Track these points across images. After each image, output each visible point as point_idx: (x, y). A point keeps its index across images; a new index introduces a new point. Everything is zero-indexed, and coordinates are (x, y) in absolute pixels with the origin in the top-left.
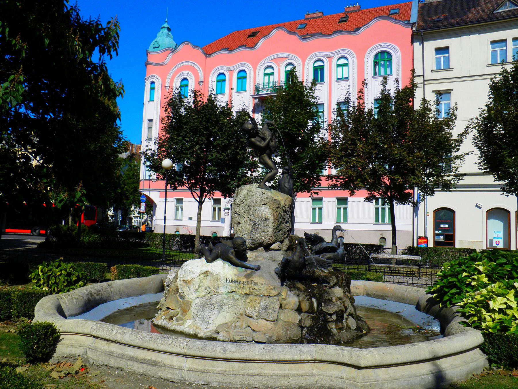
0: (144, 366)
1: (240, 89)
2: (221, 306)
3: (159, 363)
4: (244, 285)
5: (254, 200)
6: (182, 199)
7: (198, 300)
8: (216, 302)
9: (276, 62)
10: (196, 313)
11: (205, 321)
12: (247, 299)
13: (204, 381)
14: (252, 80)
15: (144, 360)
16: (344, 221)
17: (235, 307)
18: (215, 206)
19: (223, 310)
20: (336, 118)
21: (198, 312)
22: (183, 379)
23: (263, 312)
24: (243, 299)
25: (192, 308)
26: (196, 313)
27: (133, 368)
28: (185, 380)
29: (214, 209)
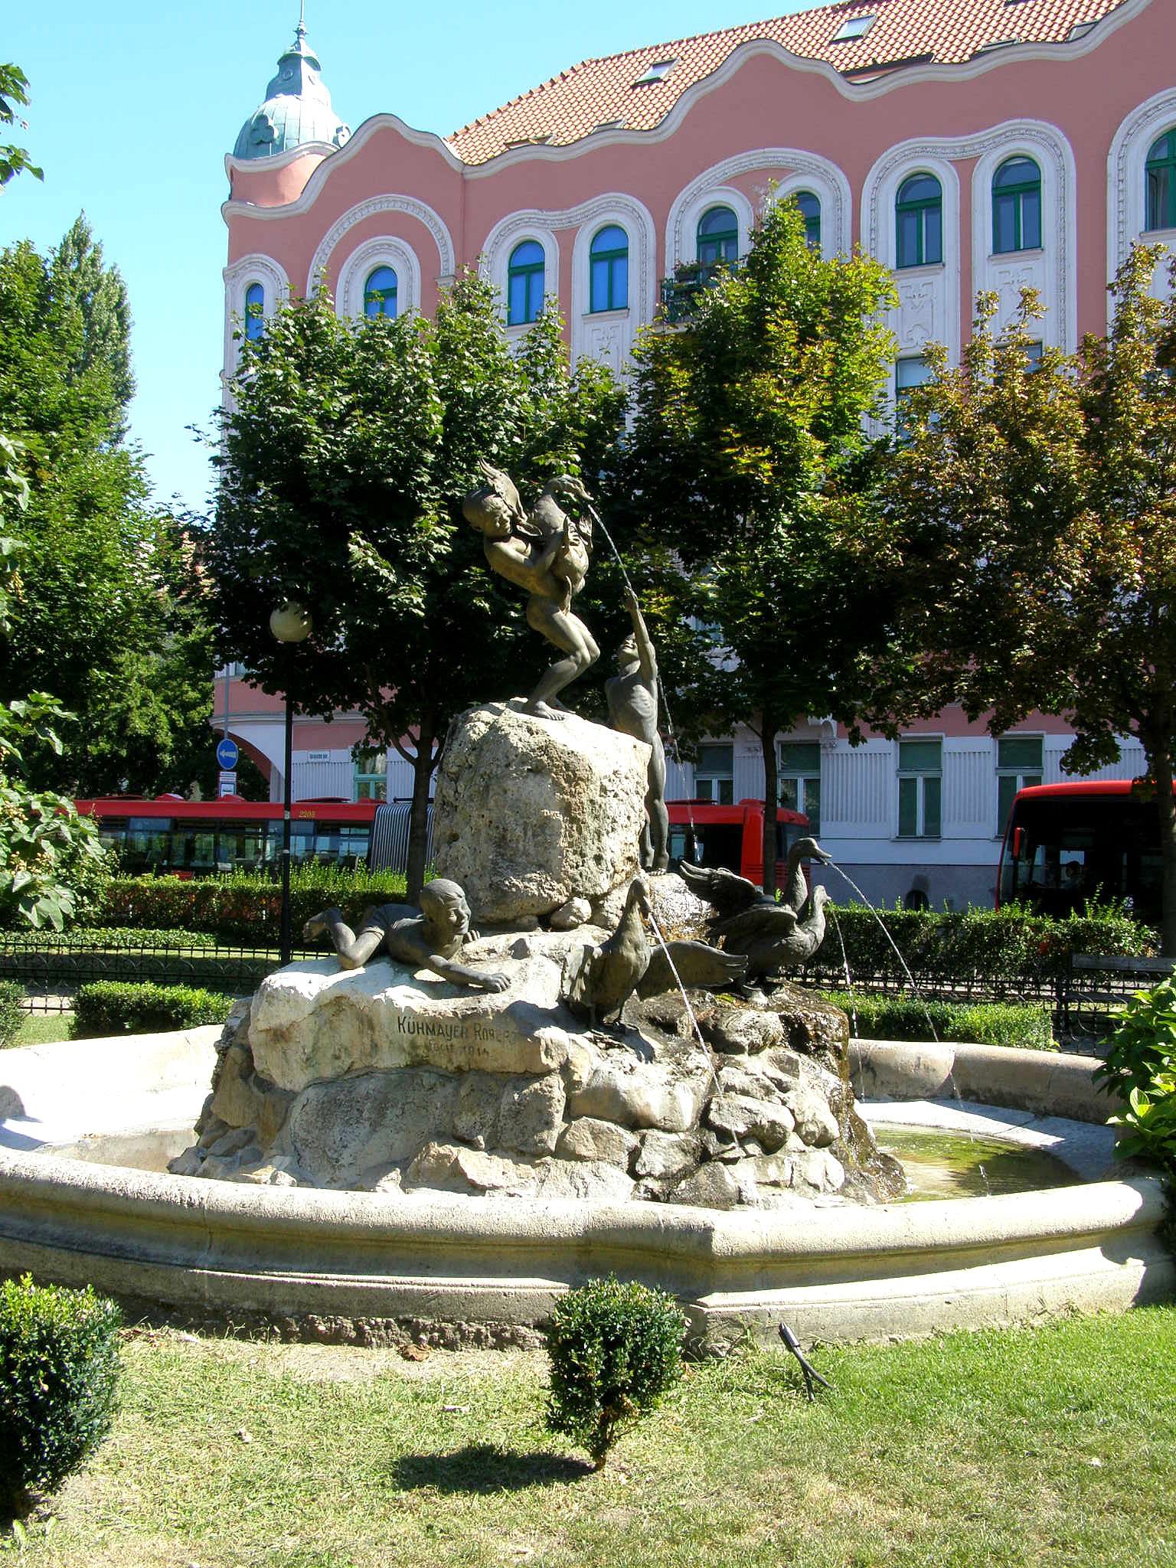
0: (89, 1259)
1: (602, 301)
2: (381, 1110)
3: (132, 1251)
4: (454, 1041)
5: (500, 756)
6: (937, 744)
7: (311, 1093)
8: (367, 1096)
9: (747, 192)
10: (302, 1134)
11: (329, 1159)
12: (460, 1085)
13: (258, 1302)
14: (651, 265)
15: (91, 1245)
16: (927, 830)
17: (423, 1112)
18: (1008, 773)
19: (386, 1121)
20: (969, 417)
21: (309, 1132)
22: (196, 1295)
23: (509, 1126)
24: (449, 1088)
25: (292, 1121)
26: (302, 1134)
27: (57, 1270)
28: (202, 1297)
29: (907, 788)
